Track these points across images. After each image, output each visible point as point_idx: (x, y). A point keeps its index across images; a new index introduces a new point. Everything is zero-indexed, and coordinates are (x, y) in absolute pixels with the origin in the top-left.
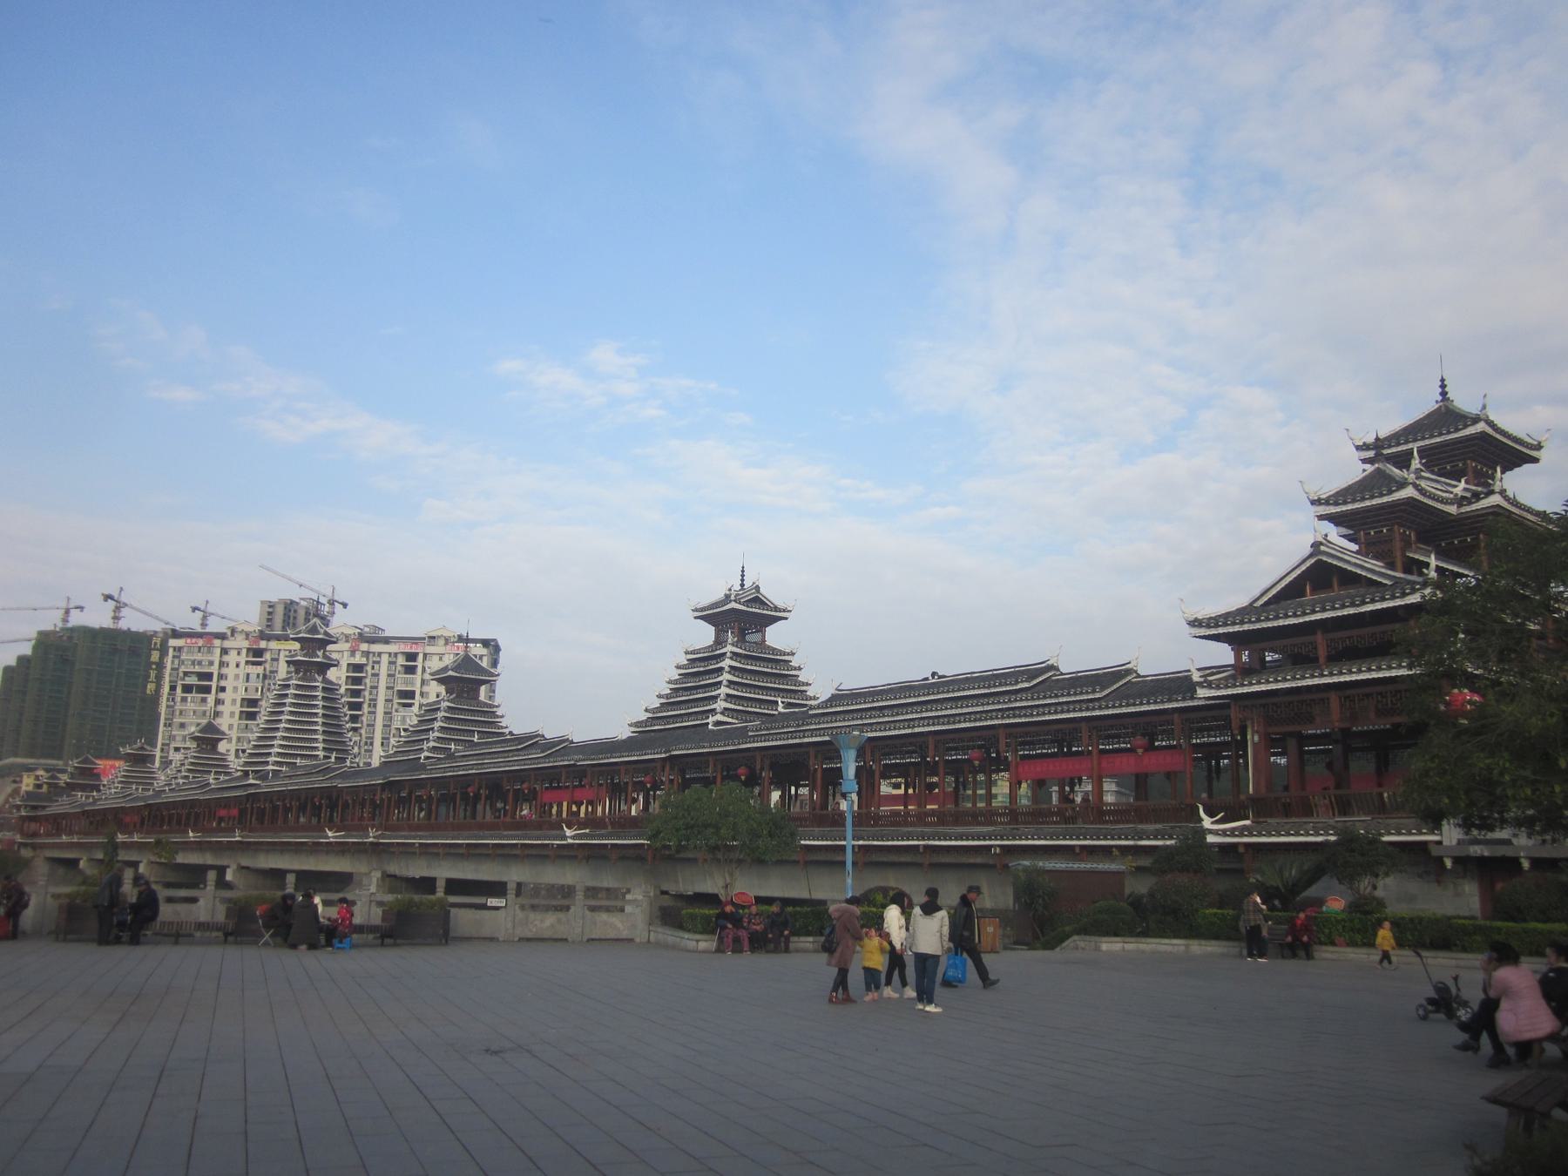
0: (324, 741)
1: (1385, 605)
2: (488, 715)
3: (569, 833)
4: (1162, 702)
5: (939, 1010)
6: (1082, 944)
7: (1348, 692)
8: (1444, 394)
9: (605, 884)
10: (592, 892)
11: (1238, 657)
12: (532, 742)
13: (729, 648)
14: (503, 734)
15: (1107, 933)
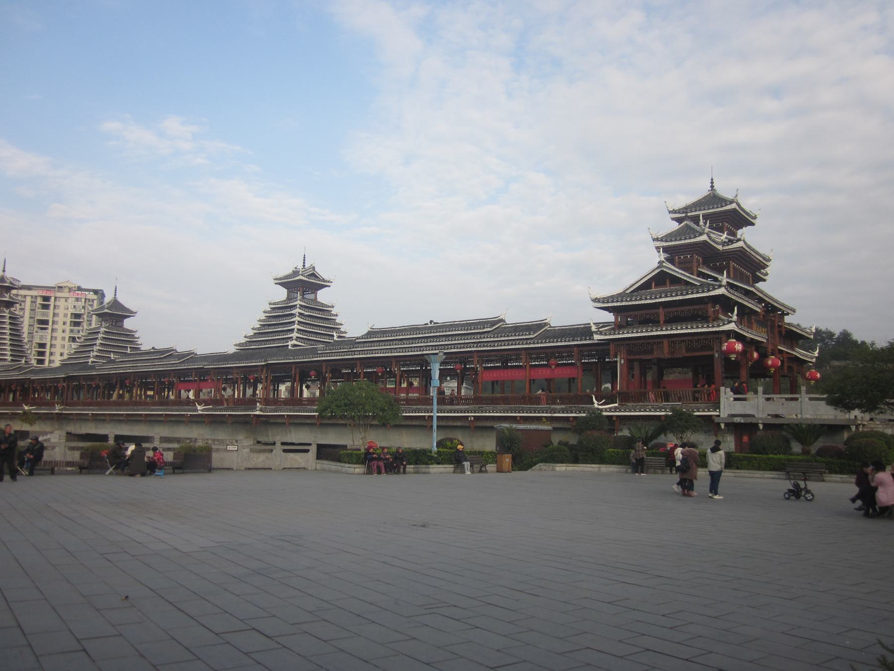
0: (11, 350)
2: (130, 337)
3: (199, 408)
5: (721, 498)
6: (544, 468)
7: (673, 339)
8: (712, 187)
9: (220, 438)
11: (616, 319)
12: (168, 354)
13: (298, 302)
15: (558, 462)
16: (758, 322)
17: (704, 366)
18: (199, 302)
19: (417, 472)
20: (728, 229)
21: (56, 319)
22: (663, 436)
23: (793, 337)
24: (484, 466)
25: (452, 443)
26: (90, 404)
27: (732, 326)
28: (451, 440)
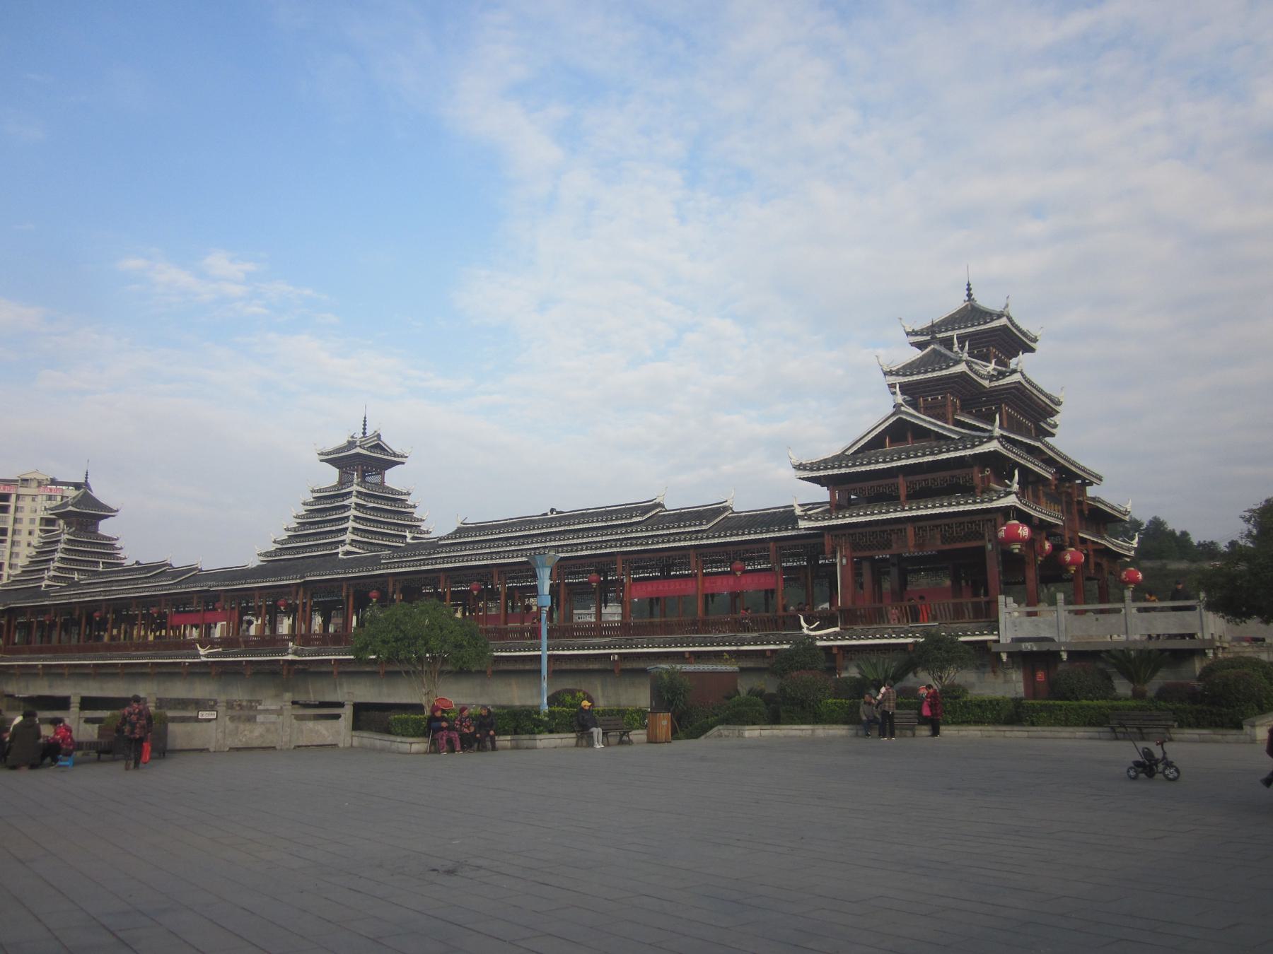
1: (958, 454)
3: (202, 651)
4: (761, 533)
6: (726, 733)
7: (921, 524)
8: (969, 295)
10: (361, 710)
11: (832, 496)
12: (158, 570)
13: (355, 488)
14: (121, 565)
15: (747, 723)
16: (1046, 494)
17: (970, 567)
18: (209, 488)
19: (516, 748)
20: (996, 356)
21: (18, 526)
22: (911, 675)
23: (1102, 518)
24: (626, 733)
25: (574, 697)
26: (41, 651)
27: (1011, 500)
28: (572, 693)
